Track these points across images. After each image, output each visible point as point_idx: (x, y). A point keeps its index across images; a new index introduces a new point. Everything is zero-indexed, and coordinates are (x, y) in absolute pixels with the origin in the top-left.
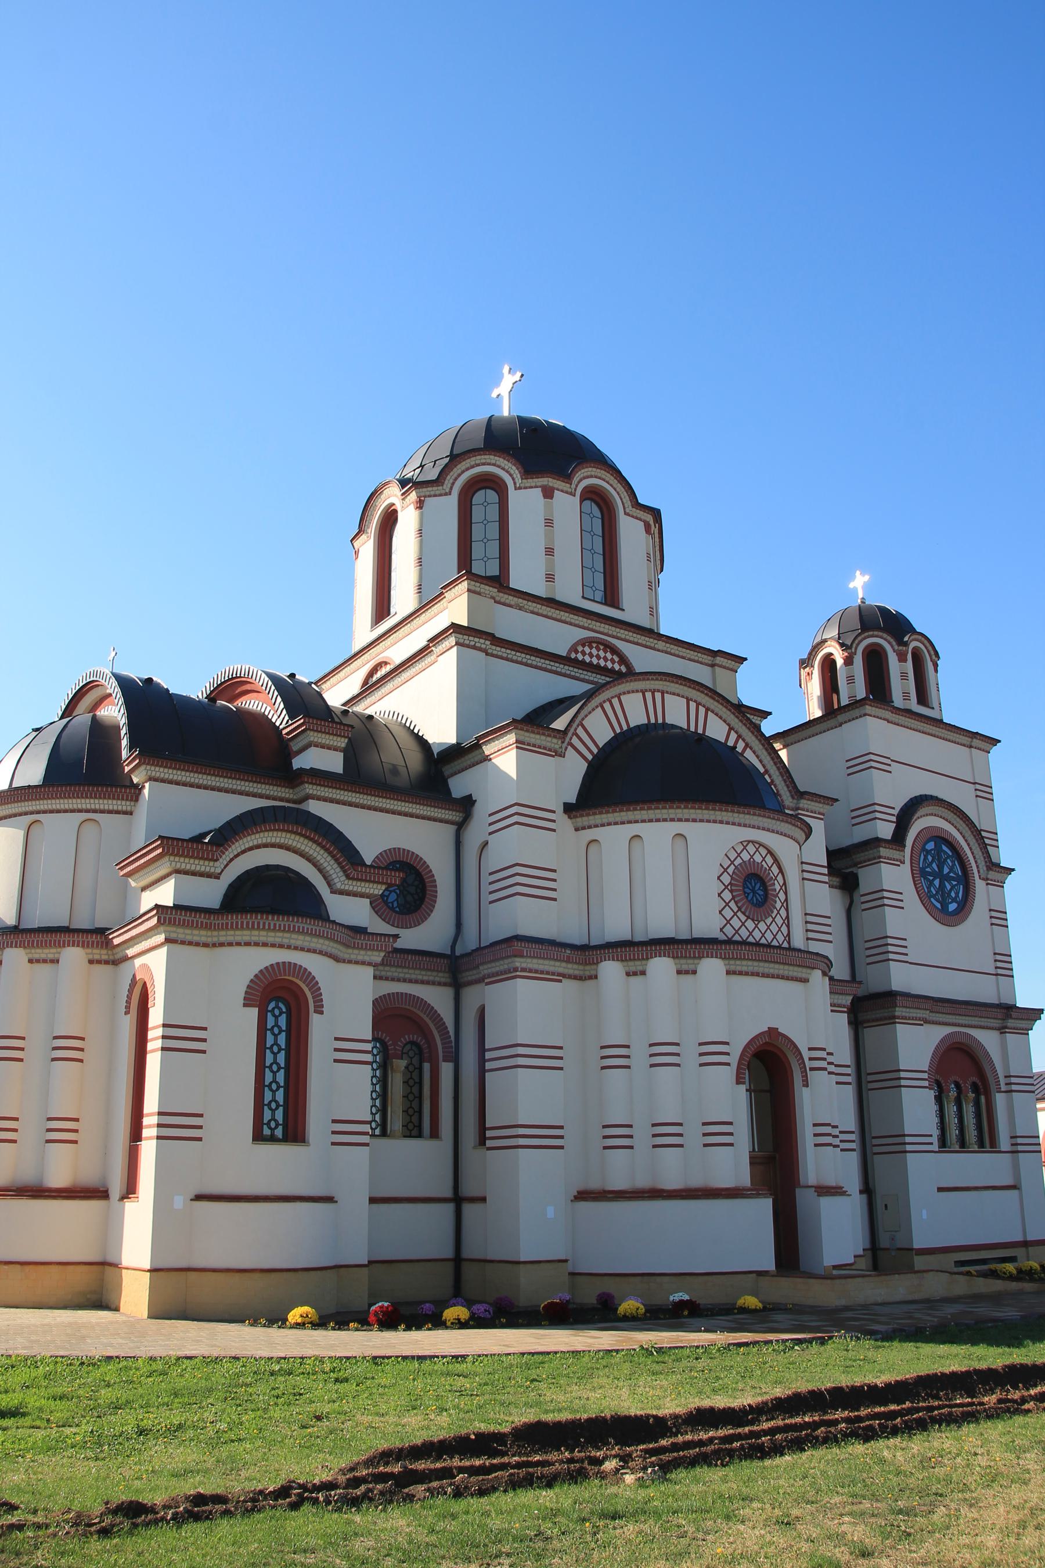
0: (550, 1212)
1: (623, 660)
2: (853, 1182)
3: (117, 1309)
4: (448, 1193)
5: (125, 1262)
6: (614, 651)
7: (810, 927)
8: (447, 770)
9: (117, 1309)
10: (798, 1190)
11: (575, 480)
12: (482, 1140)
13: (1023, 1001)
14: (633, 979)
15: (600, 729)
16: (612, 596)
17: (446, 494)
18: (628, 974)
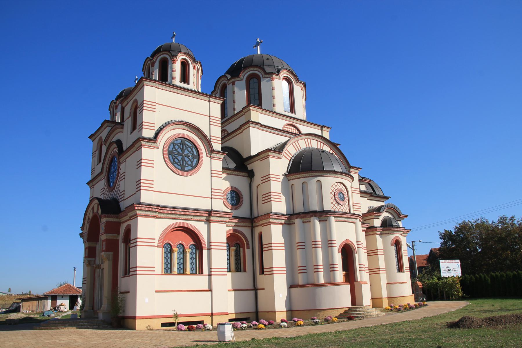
0: (147, 300)
1: (298, 130)
2: (368, 282)
3: (135, 330)
4: (251, 287)
5: (138, 315)
6: (294, 126)
7: (355, 207)
8: (246, 163)
9: (135, 330)
10: (355, 283)
11: (281, 75)
12: (262, 272)
13: (233, 292)
14: (306, 224)
15: (291, 151)
16: (293, 109)
18: (303, 222)
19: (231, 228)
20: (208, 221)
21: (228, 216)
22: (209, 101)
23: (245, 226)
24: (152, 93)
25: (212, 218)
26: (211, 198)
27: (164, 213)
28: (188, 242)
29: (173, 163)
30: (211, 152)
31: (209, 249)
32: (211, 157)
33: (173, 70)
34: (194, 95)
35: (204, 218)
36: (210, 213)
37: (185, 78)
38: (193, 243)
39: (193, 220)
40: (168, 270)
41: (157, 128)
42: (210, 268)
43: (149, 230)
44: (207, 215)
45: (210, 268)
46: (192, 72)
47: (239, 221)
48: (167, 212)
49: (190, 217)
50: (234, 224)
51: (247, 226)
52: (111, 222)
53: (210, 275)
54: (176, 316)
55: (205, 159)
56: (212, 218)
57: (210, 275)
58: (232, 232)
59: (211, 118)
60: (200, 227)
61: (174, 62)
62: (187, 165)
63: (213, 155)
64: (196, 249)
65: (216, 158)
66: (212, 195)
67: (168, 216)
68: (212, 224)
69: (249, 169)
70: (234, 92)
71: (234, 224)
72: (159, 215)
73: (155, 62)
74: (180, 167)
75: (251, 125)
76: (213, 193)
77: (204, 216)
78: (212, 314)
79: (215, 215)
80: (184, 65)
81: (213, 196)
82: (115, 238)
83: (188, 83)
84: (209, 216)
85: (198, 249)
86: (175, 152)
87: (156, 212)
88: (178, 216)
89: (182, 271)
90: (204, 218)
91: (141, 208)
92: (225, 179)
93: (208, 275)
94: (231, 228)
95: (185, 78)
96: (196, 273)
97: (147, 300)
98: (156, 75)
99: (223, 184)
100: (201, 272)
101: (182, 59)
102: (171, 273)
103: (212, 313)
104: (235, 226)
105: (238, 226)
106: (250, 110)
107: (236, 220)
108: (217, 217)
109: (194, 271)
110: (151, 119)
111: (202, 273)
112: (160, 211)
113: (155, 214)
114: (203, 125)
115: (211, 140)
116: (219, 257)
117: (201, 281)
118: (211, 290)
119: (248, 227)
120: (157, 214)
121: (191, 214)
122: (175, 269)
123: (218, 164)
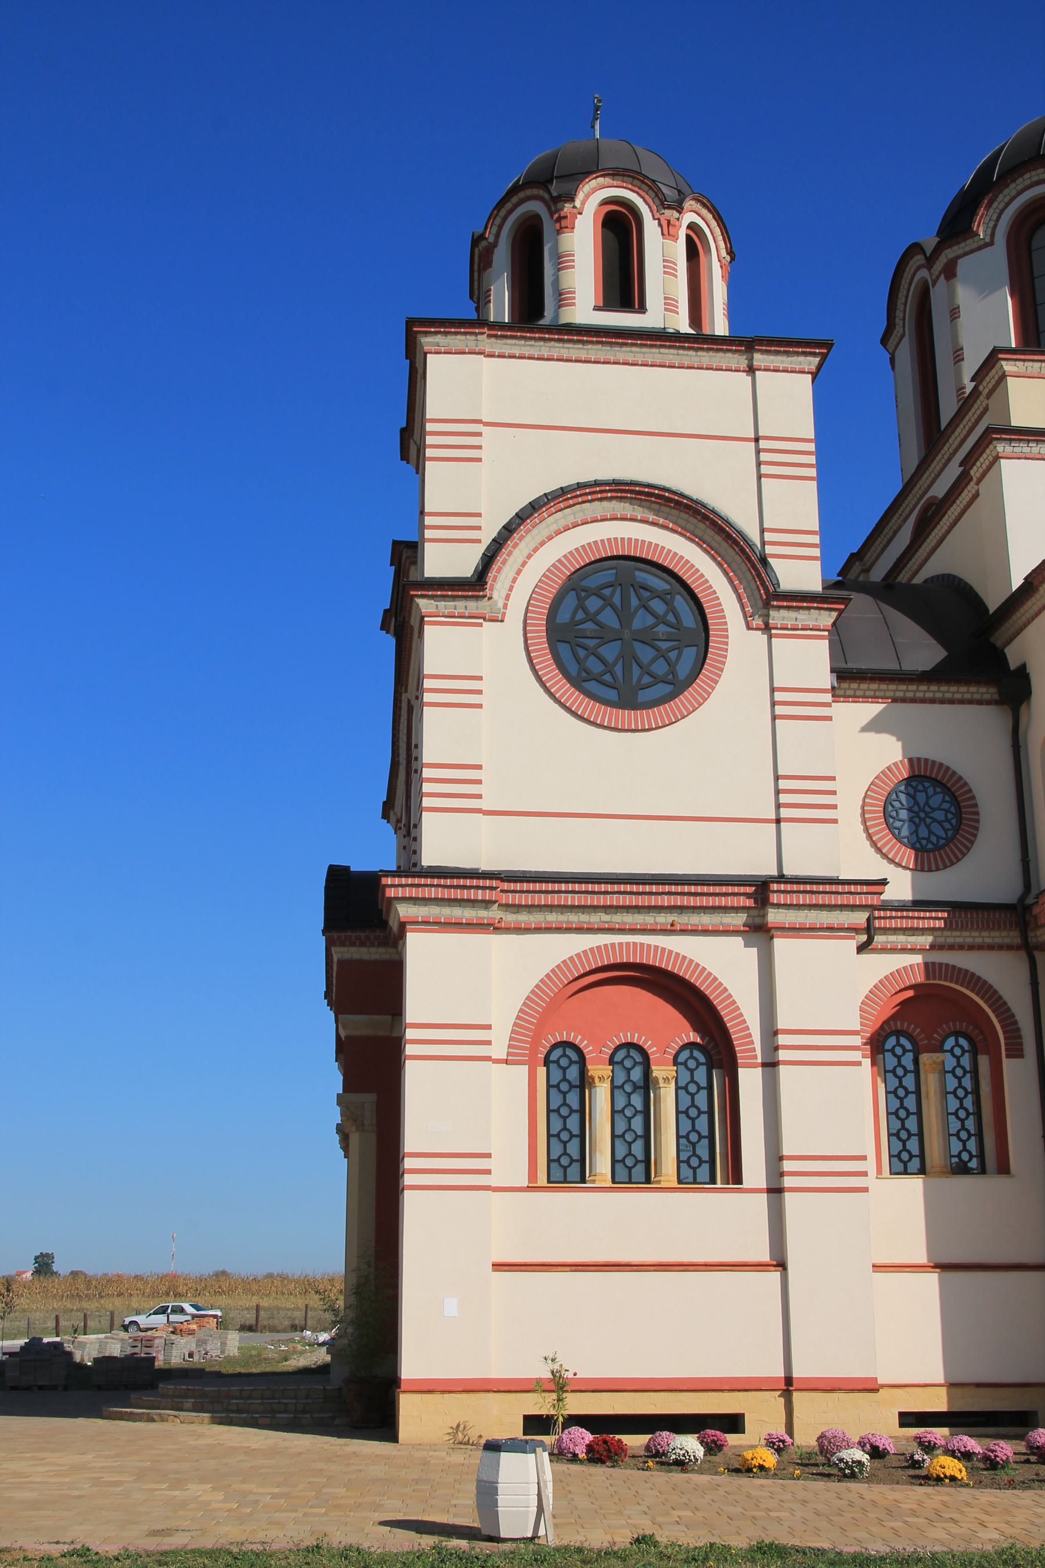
0: (451, 1307)
13: (932, 1280)
17: (987, 245)
19: (918, 959)
20: (759, 932)
21: (857, 900)
22: (751, 370)
23: (991, 947)
24: (460, 380)
25: (774, 917)
26: (778, 821)
27: (530, 908)
28: (667, 1031)
29: (580, 680)
30: (767, 605)
31: (771, 1065)
32: (767, 628)
33: (561, 261)
34: (669, 355)
35: (738, 920)
36: (761, 889)
37: (623, 284)
38: (694, 1037)
39: (684, 932)
40: (565, 1164)
41: (488, 535)
42: (775, 1157)
43: (466, 985)
44: (749, 903)
45: (775, 1157)
46: (661, 254)
47: (949, 925)
48: (543, 899)
49: (663, 919)
50: (926, 940)
51: (1000, 947)
52: (361, 962)
53: (775, 1191)
54: (559, 1385)
55: (739, 642)
56: (774, 917)
57: (775, 1191)
58: (920, 978)
59: (763, 444)
60: (722, 962)
61: (563, 224)
62: (646, 679)
63: (777, 617)
64: (710, 1066)
65: (793, 631)
66: (778, 806)
67: (553, 918)
68: (781, 945)
69: (1013, 665)
70: (954, 313)
71: (926, 940)
72: (510, 918)
73: (495, 245)
74: (612, 695)
75: (1000, 448)
76: (784, 798)
77: (736, 909)
78: (788, 1386)
79: (783, 899)
80: (620, 231)
81: (784, 813)
82: (381, 1033)
83: (642, 309)
84: (758, 904)
85: (720, 1066)
86: (589, 625)
87: (487, 904)
88: (605, 918)
89: (635, 1170)
90: (738, 920)
91: (414, 892)
92: (874, 726)
93: (769, 1191)
94: (918, 959)
95: (623, 284)
96: (713, 1181)
97: (451, 1307)
98: (501, 304)
99: (861, 749)
100: (735, 1175)
101: (606, 202)
102: (648, 1180)
103: (789, 1380)
104: (933, 947)
105: (951, 947)
106: (1003, 376)
107: (937, 920)
108: (799, 907)
109: (704, 1172)
110: (463, 496)
111: (737, 1178)
112: (510, 899)
113: (483, 914)
114: (722, 483)
115: (769, 550)
116: (829, 1105)
117: (729, 1220)
118: (781, 1265)
119: (1010, 947)
120: (494, 913)
121: (666, 901)
122: (602, 1164)
123: (807, 659)
